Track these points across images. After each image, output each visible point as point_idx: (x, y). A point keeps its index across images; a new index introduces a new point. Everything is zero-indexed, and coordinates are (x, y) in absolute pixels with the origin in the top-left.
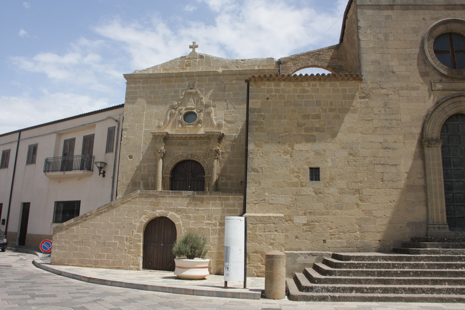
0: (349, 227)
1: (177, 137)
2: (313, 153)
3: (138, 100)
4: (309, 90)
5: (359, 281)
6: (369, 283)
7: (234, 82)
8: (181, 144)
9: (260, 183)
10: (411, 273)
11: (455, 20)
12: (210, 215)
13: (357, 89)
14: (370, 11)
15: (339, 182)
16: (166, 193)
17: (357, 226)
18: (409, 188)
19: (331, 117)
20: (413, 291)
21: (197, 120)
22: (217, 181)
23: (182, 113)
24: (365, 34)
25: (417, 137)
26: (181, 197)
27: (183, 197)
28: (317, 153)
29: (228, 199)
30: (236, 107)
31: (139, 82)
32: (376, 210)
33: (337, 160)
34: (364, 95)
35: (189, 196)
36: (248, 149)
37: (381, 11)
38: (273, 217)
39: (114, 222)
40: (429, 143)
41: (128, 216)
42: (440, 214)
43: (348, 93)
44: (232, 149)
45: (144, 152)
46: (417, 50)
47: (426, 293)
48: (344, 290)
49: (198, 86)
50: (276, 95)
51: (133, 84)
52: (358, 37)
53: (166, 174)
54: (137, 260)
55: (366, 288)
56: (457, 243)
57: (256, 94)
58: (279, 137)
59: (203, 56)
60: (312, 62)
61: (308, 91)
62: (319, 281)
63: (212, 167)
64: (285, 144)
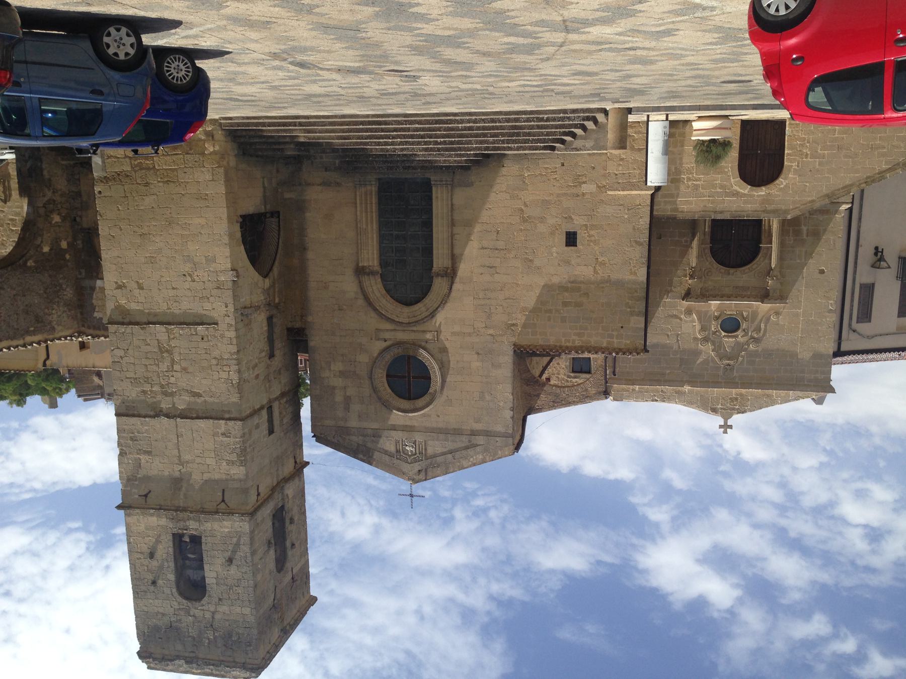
2: (573, 262)
5: (539, 127)
7: (668, 372)
9: (634, 229)
14: (498, 430)
16: (751, 215)
17: (527, 182)
18: (469, 224)
20: (493, 121)
25: (457, 280)
26: (732, 212)
27: (729, 211)
28: (568, 262)
34: (512, 328)
36: (646, 268)
37: (485, 429)
40: (446, 272)
42: (439, 195)
43: (530, 330)
46: (449, 379)
48: (554, 119)
50: (612, 331)
51: (820, 378)
54: (792, 131)
55: (534, 121)
60: (564, 392)
62: (576, 126)
63: (699, 256)
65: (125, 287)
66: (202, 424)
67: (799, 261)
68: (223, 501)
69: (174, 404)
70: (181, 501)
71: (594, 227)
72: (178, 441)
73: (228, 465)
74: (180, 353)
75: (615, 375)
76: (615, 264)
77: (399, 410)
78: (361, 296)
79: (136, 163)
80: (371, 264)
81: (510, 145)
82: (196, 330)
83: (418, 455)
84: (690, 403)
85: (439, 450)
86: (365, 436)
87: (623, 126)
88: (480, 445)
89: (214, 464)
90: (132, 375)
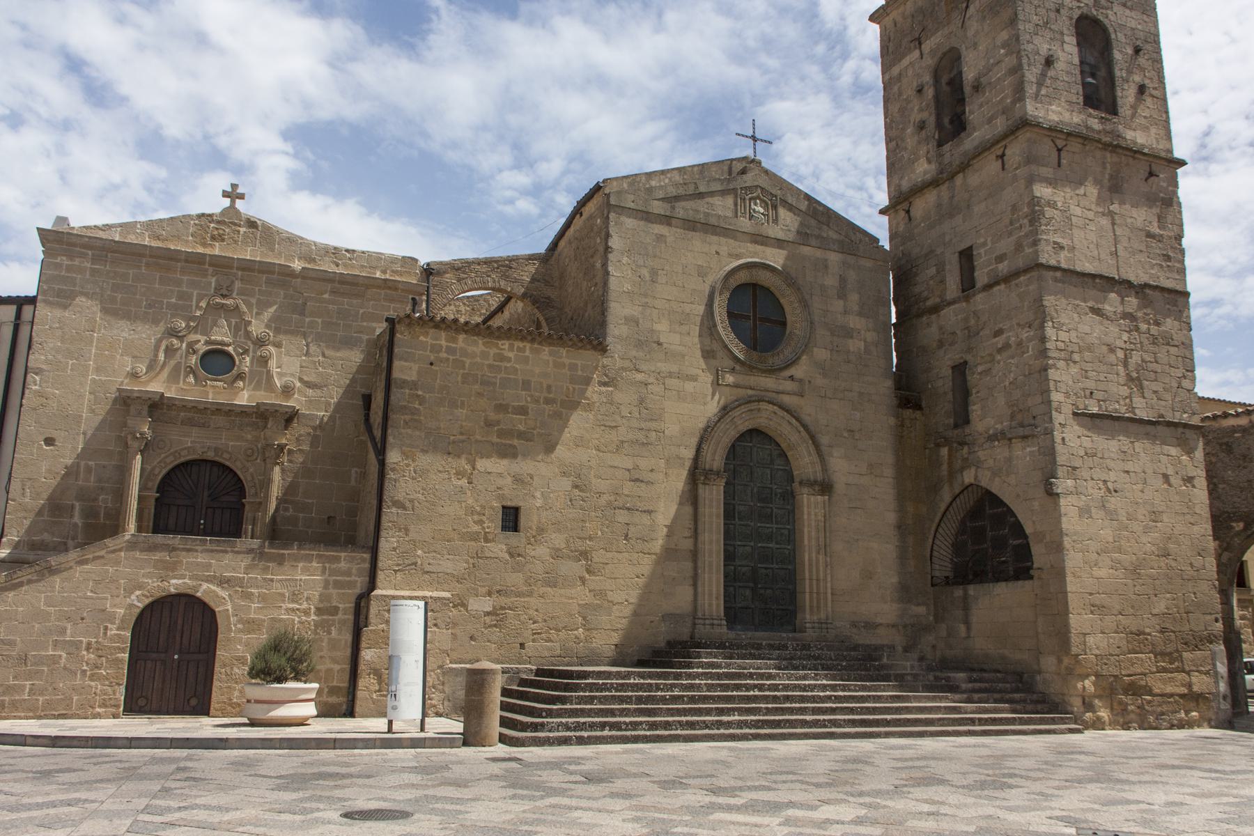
0: (567, 619)
1: (184, 406)
2: (509, 480)
3: (77, 299)
4: (511, 358)
5: (612, 713)
6: (626, 716)
7: (326, 296)
8: (190, 423)
9: (407, 530)
10: (685, 699)
11: (764, 264)
12: (296, 592)
13: (596, 368)
14: (631, 220)
15: (554, 536)
16: (198, 542)
17: (580, 618)
18: (669, 553)
19: (546, 414)
20: (691, 725)
21: (235, 371)
22: (274, 517)
23: (198, 350)
24: (618, 264)
25: (688, 464)
26: (232, 551)
27: (238, 553)
28: (518, 480)
29: (337, 559)
30: (327, 352)
31: (83, 256)
32: (612, 591)
33: (552, 495)
34: (607, 380)
35: (250, 551)
36: (387, 461)
37: (650, 225)
38: (431, 597)
39: (56, 606)
40: (706, 478)
41: (95, 593)
42: (714, 602)
43: (580, 373)
44: (312, 445)
45: (90, 433)
46: (701, 309)
47: (710, 728)
48: (592, 726)
49: (241, 293)
50: (448, 359)
51: (64, 258)
52: (605, 265)
53: (148, 489)
55: (625, 723)
56: (744, 652)
57: (409, 350)
58: (449, 443)
59: (256, 222)
60: (494, 282)
61: (509, 360)
64: (459, 457)
65: (1183, 480)
66: (1089, 268)
67: (90, 463)
68: (1059, 150)
69: (1122, 302)
70: (1109, 160)
71: (474, 537)
72: (1116, 247)
73: (1055, 202)
74: (1118, 374)
75: (413, 299)
76: (440, 472)
77: (772, 269)
78: (824, 449)
79: (1176, 664)
80: (812, 498)
81: (642, 681)
82: (1100, 406)
83: (747, 197)
84: (292, 240)
85: (717, 201)
86: (818, 237)
87: (472, 710)
88: (659, 200)
89: (1072, 207)
90: (1173, 350)
